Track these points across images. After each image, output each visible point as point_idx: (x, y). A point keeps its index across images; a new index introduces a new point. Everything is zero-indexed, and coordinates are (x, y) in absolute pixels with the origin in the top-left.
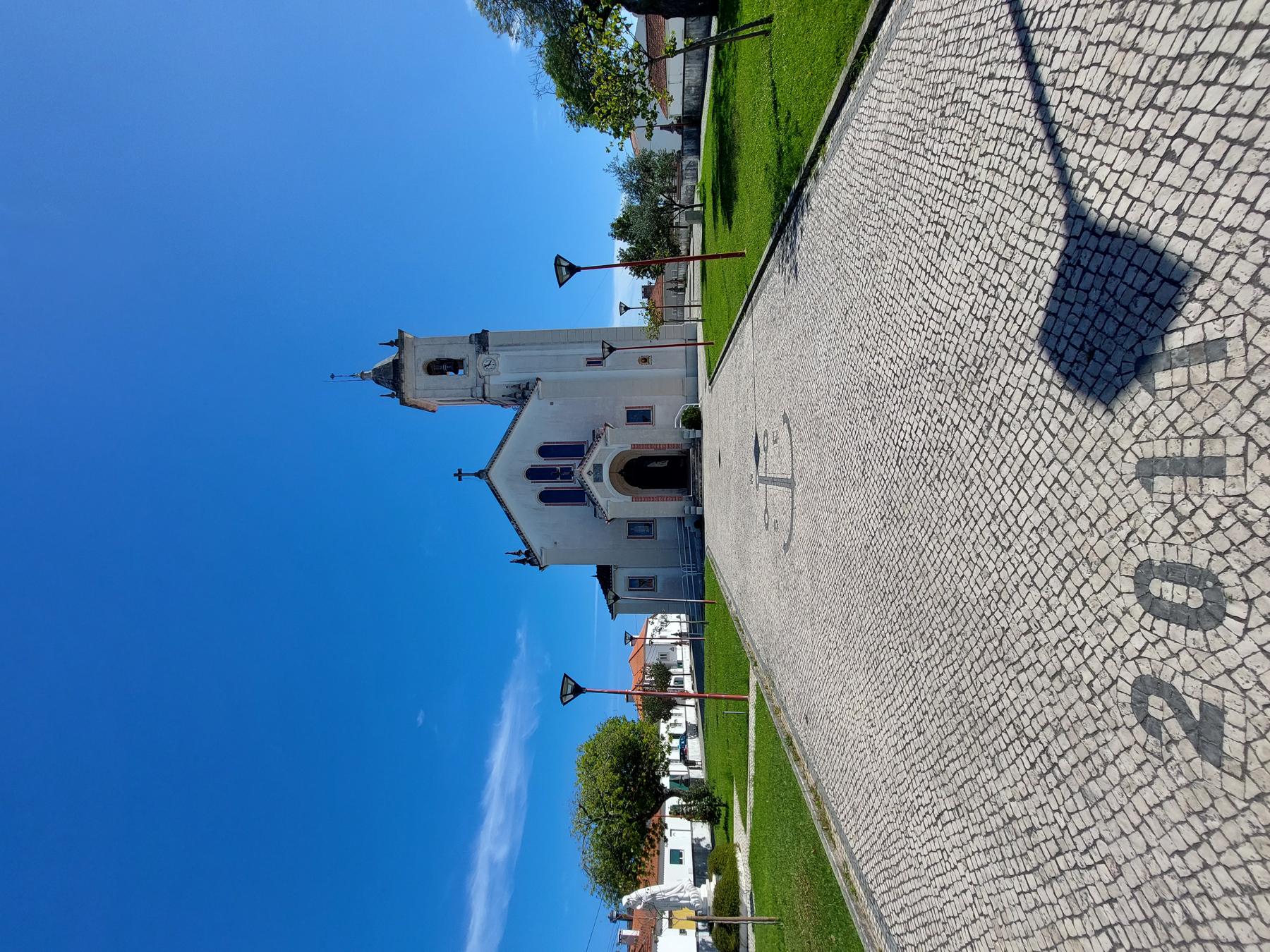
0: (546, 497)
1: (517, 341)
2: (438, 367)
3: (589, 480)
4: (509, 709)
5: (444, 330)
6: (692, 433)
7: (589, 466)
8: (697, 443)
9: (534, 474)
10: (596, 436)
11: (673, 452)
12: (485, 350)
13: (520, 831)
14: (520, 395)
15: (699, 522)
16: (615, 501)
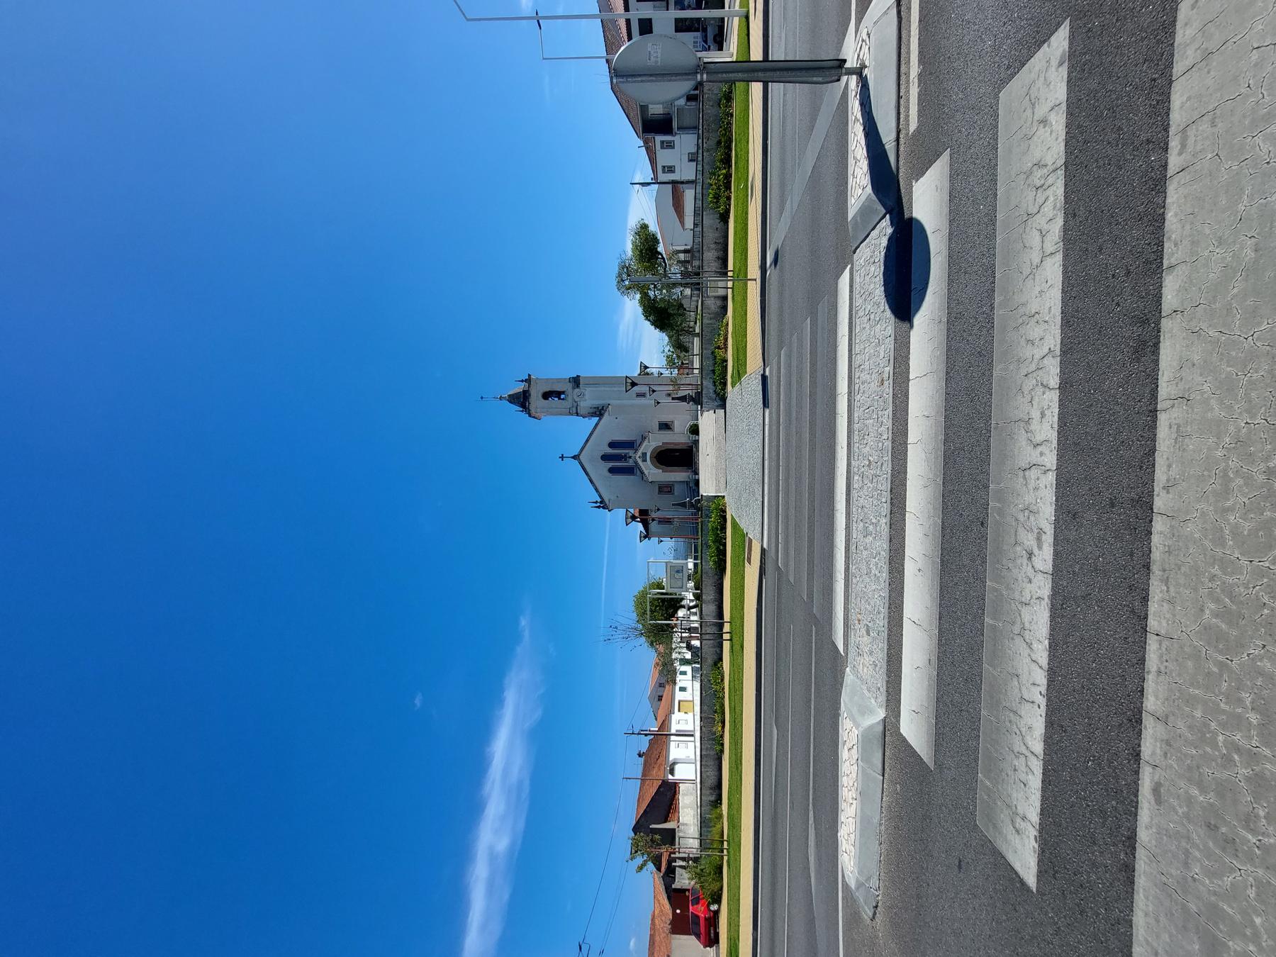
0: (612, 470)
1: (598, 382)
2: (546, 395)
3: (640, 461)
4: (511, 698)
5: (554, 370)
6: (694, 437)
7: (639, 453)
8: (696, 442)
9: (605, 458)
10: (644, 438)
11: (684, 447)
12: (578, 386)
13: (521, 824)
14: (599, 412)
15: (697, 483)
16: (653, 472)
